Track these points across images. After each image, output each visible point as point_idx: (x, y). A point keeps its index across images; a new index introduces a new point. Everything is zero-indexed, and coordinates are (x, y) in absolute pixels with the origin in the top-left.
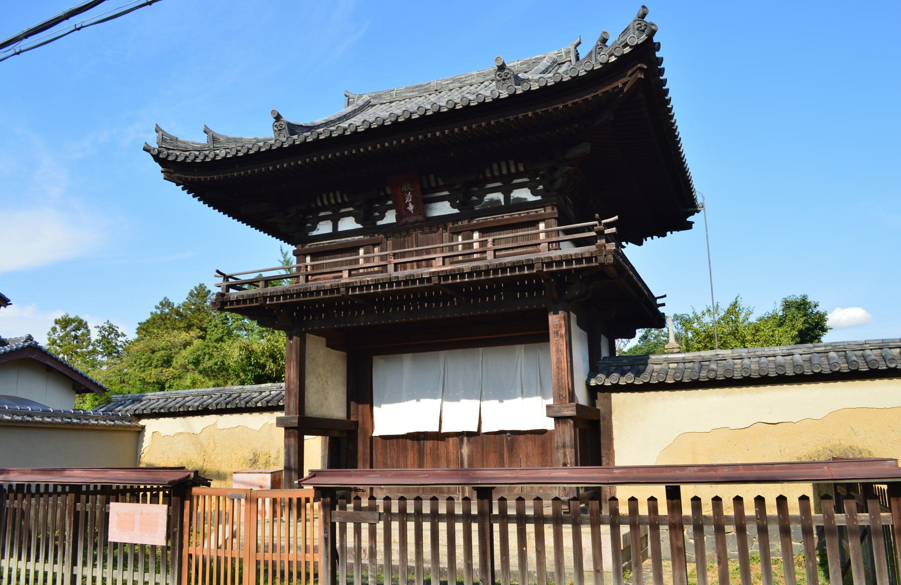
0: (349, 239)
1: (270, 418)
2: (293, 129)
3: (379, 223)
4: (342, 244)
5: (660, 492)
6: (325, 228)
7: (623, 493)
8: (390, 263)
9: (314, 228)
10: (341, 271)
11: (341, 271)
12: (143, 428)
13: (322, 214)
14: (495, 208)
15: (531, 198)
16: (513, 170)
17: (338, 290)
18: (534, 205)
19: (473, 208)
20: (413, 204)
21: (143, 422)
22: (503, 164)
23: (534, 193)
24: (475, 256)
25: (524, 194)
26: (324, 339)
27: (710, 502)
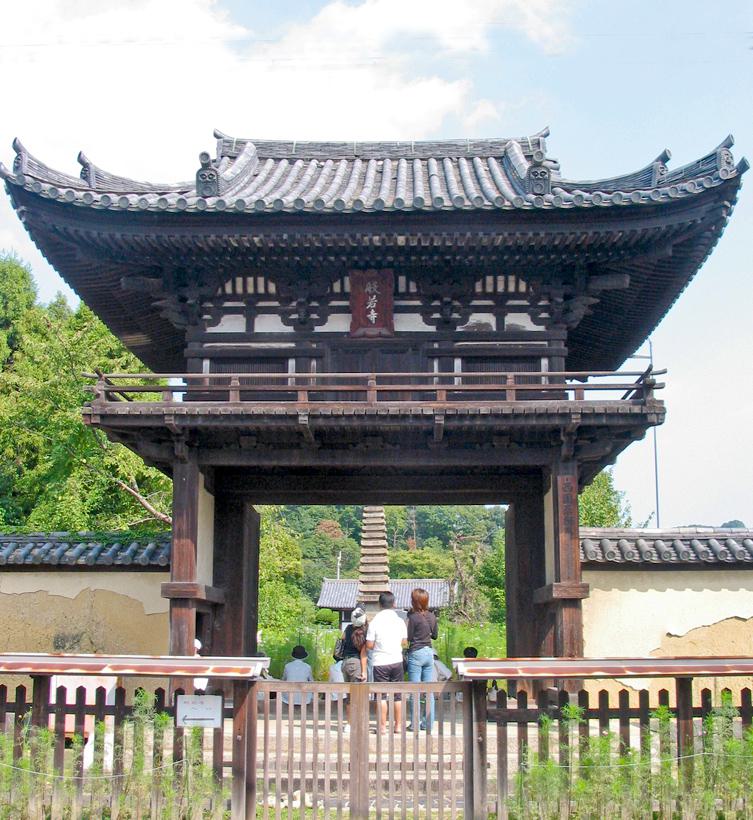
3: (318, 329)
5: (670, 685)
6: (232, 324)
7: (593, 688)
8: (370, 388)
9: (215, 322)
14: (482, 333)
15: (531, 327)
20: (376, 310)
22: (501, 279)
23: (536, 321)
25: (521, 321)
27: (740, 694)
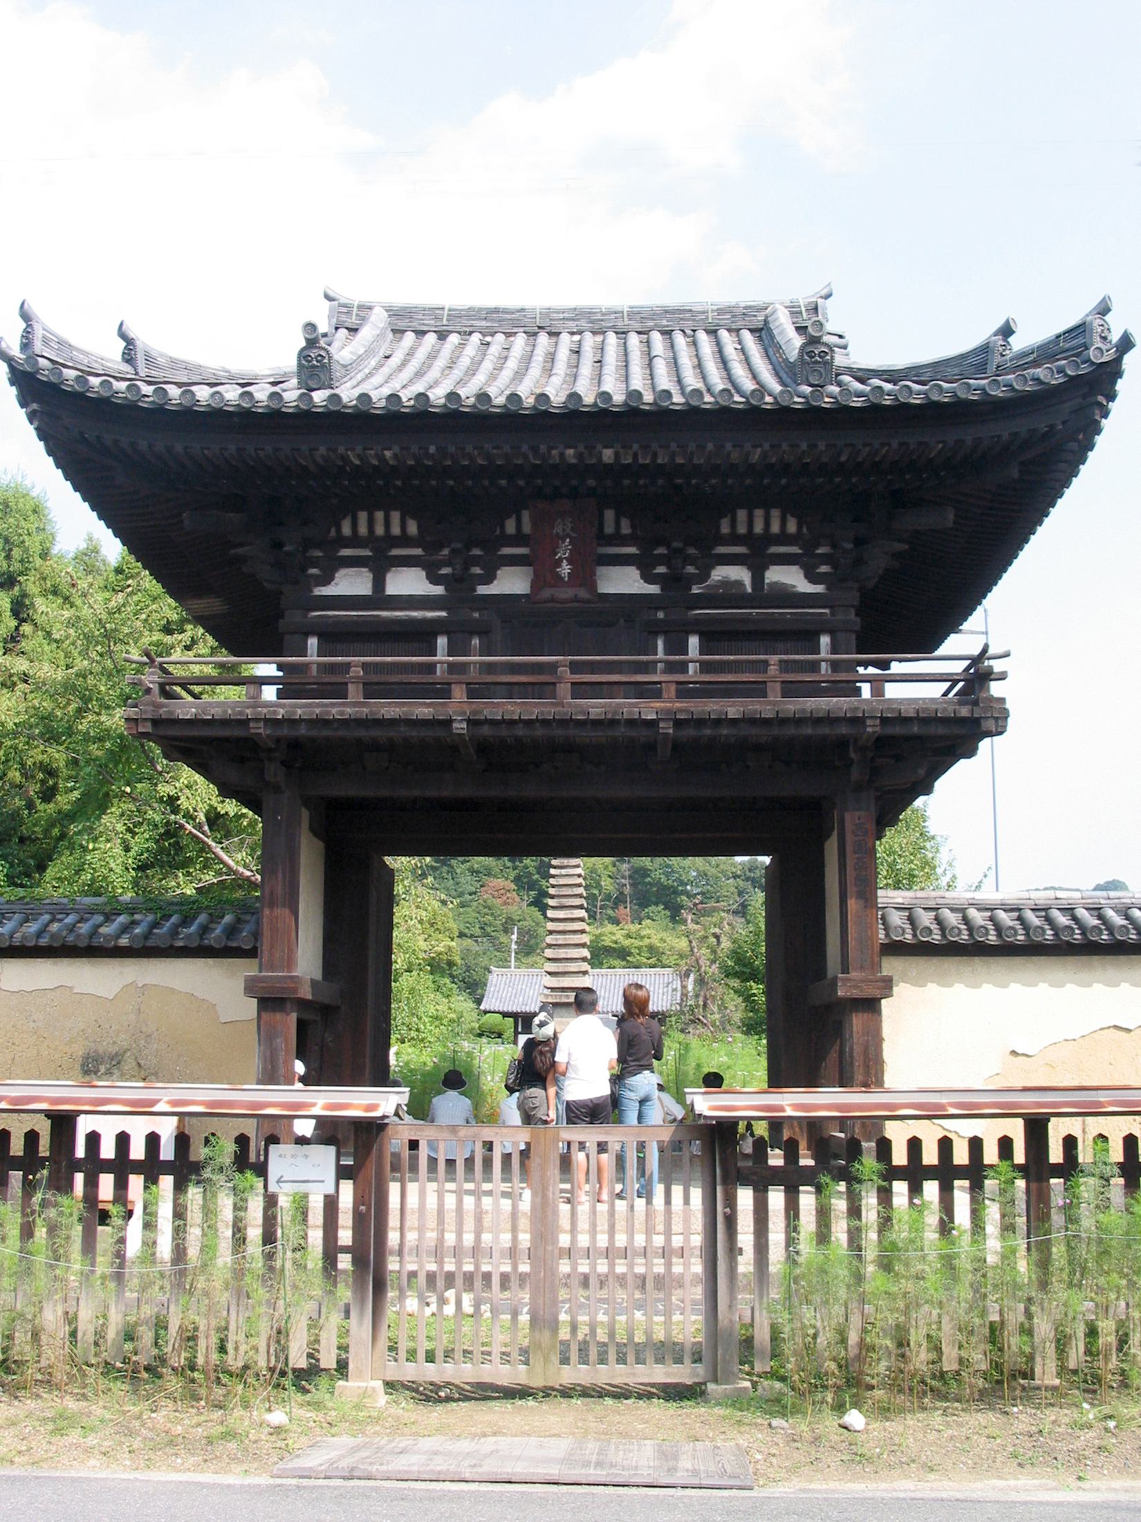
0: (415, 614)
3: (482, 590)
4: (745, 620)
6: (351, 583)
9: (327, 580)
14: (729, 595)
16: (396, 530)
23: (812, 577)
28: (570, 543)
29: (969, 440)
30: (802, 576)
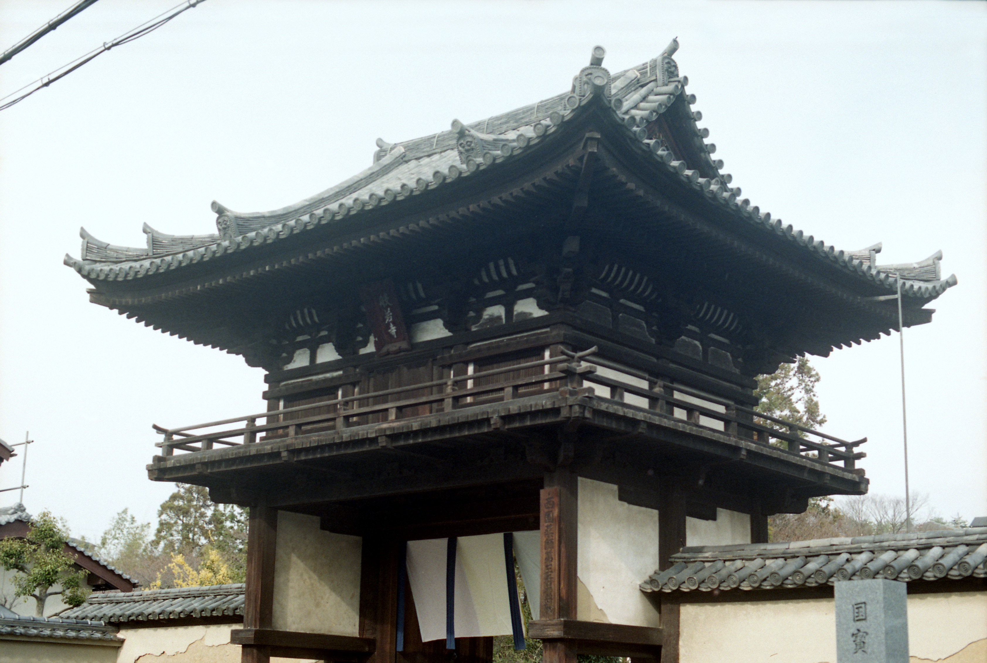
0: (328, 375)
1: (223, 632)
2: (243, 223)
10: (502, 389)
11: (502, 389)
12: (122, 641)
13: (490, 295)
14: (495, 329)
17: (488, 420)
18: (540, 323)
19: (468, 330)
20: (394, 324)
21: (121, 635)
24: (469, 400)
25: (529, 307)
26: (615, 487)
28: (391, 311)
29: (916, 287)
30: (535, 304)
